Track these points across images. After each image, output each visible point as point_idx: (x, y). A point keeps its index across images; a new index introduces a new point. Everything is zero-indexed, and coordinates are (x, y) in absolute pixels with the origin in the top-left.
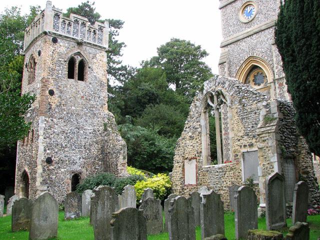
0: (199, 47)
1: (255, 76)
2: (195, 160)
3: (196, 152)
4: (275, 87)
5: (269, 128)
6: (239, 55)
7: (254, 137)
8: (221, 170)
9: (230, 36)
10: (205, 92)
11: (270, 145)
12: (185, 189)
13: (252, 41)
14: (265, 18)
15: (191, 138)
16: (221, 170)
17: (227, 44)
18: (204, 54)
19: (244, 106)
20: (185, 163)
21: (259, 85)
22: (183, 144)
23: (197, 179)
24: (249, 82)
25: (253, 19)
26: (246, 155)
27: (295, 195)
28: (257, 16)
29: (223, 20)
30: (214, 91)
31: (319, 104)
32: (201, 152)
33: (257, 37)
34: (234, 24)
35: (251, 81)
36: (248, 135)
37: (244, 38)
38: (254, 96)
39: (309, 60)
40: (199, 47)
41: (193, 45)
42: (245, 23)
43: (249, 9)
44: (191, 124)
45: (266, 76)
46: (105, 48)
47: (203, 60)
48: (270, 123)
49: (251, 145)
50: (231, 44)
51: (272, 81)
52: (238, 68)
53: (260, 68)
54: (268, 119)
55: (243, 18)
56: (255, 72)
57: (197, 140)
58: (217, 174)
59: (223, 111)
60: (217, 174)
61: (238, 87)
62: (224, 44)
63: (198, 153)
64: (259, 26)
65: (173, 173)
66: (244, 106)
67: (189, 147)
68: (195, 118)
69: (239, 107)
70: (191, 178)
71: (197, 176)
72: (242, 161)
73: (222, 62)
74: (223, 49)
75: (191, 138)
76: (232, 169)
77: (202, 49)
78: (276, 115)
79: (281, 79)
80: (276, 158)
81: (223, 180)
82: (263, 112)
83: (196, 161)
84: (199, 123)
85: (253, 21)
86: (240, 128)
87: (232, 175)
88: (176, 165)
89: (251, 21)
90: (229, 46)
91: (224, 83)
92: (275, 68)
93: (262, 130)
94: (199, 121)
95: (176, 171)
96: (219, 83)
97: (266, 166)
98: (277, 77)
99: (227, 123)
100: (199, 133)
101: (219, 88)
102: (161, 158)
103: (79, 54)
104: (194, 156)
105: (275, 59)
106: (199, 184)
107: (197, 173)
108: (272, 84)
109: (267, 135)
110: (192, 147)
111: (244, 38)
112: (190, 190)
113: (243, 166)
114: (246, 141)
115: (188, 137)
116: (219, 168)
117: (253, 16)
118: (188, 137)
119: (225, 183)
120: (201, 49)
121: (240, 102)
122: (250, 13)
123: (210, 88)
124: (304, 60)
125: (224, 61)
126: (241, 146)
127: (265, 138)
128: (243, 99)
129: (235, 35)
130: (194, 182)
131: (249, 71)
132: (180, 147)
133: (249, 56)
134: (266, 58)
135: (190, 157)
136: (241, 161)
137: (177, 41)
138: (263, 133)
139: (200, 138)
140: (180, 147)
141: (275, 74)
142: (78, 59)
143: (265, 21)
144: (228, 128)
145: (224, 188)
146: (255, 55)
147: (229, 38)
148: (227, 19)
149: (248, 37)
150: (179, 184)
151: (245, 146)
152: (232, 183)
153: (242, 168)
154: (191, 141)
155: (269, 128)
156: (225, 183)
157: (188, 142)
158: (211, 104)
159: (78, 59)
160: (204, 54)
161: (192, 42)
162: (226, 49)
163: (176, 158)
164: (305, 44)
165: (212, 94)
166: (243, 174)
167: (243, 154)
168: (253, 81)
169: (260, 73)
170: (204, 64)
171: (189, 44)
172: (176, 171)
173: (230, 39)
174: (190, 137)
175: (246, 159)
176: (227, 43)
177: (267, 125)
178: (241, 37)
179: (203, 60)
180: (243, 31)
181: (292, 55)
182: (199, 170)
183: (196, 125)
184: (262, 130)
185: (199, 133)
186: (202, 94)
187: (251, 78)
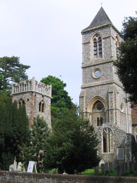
4: (109, 113)
9: (86, 83)
13: (98, 88)
17: (85, 87)
18: (65, 85)
21: (100, 110)
31: (136, 44)
34: (89, 78)
35: (96, 108)
37: (94, 86)
40: (62, 82)
42: (95, 79)
46: (50, 97)
51: (107, 109)
56: (98, 104)
62: (83, 87)
74: (83, 89)
79: (112, 110)
103: (43, 100)
108: (107, 111)
111: (94, 86)
136: (100, 142)
137: (51, 77)
141: (109, 107)
142: (42, 102)
146: (99, 96)
147: (86, 84)
148: (86, 74)
149: (97, 86)
159: (42, 102)
162: (85, 90)
165: (106, 128)
178: (93, 85)
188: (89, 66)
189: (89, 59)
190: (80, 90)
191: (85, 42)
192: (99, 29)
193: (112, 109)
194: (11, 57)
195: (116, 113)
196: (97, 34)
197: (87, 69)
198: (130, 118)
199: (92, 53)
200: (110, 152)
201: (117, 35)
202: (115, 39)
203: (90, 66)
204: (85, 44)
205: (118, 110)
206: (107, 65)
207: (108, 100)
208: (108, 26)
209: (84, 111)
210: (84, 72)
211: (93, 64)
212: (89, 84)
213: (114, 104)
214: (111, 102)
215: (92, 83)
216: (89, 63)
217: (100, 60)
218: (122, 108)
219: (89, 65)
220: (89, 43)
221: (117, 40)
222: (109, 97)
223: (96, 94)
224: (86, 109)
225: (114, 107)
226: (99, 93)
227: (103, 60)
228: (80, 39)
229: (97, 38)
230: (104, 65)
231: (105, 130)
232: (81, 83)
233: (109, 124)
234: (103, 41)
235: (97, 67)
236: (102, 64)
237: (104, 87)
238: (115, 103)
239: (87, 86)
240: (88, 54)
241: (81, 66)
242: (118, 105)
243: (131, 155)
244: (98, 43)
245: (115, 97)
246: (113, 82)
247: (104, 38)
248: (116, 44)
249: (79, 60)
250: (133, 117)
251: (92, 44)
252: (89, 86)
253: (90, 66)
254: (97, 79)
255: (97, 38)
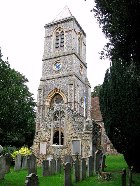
0: (24, 76)
1: (56, 99)
2: (46, 142)
3: (47, 138)
5: (89, 132)
6: (50, 87)
7: (79, 134)
8: (60, 148)
10: (54, 110)
11: (89, 138)
12: (40, 156)
14: (66, 71)
15: (45, 131)
16: (60, 148)
17: (44, 79)
18: (27, 81)
19: (75, 120)
20: (40, 143)
22: (40, 134)
23: (47, 151)
24: (53, 101)
25: (60, 70)
26: (74, 142)
27: (102, 160)
28: (62, 69)
29: (43, 67)
30: (60, 111)
32: (50, 139)
33: (61, 79)
36: (76, 133)
37: (54, 79)
38: (80, 116)
39: (117, 110)
40: (24, 76)
41: (21, 75)
42: (55, 71)
43: (58, 64)
44: (46, 124)
45: (63, 100)
47: (25, 84)
48: (89, 130)
49: (77, 138)
50: (46, 80)
51: (66, 103)
52: (49, 93)
53: (60, 95)
54: (88, 128)
55: (54, 68)
56: (57, 97)
57: (48, 133)
58: (58, 149)
59: (38, 114)
60: (58, 149)
61: (72, 111)
62: (42, 79)
63: (48, 139)
64: (62, 74)
65: (33, 147)
66: (75, 120)
67: (43, 135)
68: (48, 122)
69: (72, 120)
70: (43, 150)
71: (47, 150)
72: (72, 145)
73: (40, 89)
74: (42, 82)
75: (45, 131)
76: (66, 148)
77: (25, 78)
78: (92, 126)
79: (71, 102)
80: (91, 144)
81: (61, 152)
82: (85, 124)
83: (47, 143)
84: (50, 125)
85: (59, 71)
86: (72, 129)
87: (66, 150)
88: (34, 143)
89: (59, 70)
90: (45, 81)
91: (65, 108)
92: (68, 97)
93: (86, 132)
94: (50, 124)
95: (35, 147)
96: (63, 108)
97: (87, 147)
98: (69, 101)
99: (39, 121)
100: (50, 129)
101: (63, 110)
102: (5, 137)
104: (46, 140)
105: (69, 92)
106: (48, 154)
107: (47, 149)
109: (88, 134)
110: (45, 136)
111: (54, 79)
112: (42, 157)
113: (72, 146)
114: (74, 135)
115: (43, 131)
116: (60, 147)
117: (60, 69)
118: (43, 131)
119: (62, 154)
120: (25, 78)
121: (73, 118)
122: (58, 67)
123: (58, 109)
124: (115, 110)
125: (42, 88)
126: (72, 138)
127: (87, 136)
128: (74, 116)
129: (49, 76)
130: (45, 153)
131: (53, 96)
132: (38, 135)
133: (55, 88)
134: (64, 91)
135: (43, 140)
138: (86, 133)
139: (50, 132)
140: (38, 135)
141: (68, 100)
143: (66, 72)
144: (40, 124)
145: (62, 156)
146: (58, 88)
148: (46, 67)
149: (56, 78)
150: (36, 153)
151: (74, 138)
152: (66, 154)
153: (72, 147)
154: (45, 133)
155: (89, 132)
156: (62, 154)
157: (43, 133)
158: (57, 116)
160: (27, 81)
161: (21, 73)
162: (43, 82)
163: (35, 140)
164: (116, 104)
165: (58, 112)
166: (72, 150)
167: (73, 141)
168: (55, 101)
169: (60, 97)
170: (26, 86)
171: (19, 74)
172: (35, 147)
173: (46, 77)
174: (44, 131)
175: (74, 143)
176: (44, 79)
177: (88, 130)
179: (25, 84)
180: (53, 74)
181: (110, 107)
182: (48, 147)
183: (49, 125)
184: (86, 132)
185: (50, 129)
186: (53, 111)
187: (55, 99)
188: (50, 59)
189: (50, 52)
190: (39, 83)
191: (47, 36)
192: (62, 23)
193: (71, 101)
195: (75, 106)
196: (59, 28)
197: (48, 61)
198: (90, 114)
199: (53, 46)
200: (62, 143)
201: (79, 31)
202: (78, 34)
203: (51, 59)
204: (47, 37)
205: (78, 103)
206: (68, 57)
207: (68, 92)
208: (71, 20)
209: (79, 154)
210: (44, 64)
211: (54, 57)
212: (49, 76)
213: (73, 96)
214: (70, 95)
215: (52, 76)
216: (50, 56)
217: (60, 52)
218: (82, 103)
219: (50, 58)
220: (52, 36)
221: (79, 36)
222: (69, 90)
223: (55, 87)
224: (44, 102)
225: (73, 99)
226: (58, 85)
227: (64, 53)
228: (43, 32)
229: (60, 32)
230: (65, 57)
231: (56, 115)
232: (40, 76)
233: (62, 106)
234: (65, 34)
235: (58, 59)
236: (63, 56)
237: (63, 80)
238: (75, 95)
239: (46, 79)
240: (50, 47)
241: (42, 58)
242: (78, 98)
243: (91, 148)
244: (59, 37)
245: (75, 90)
246: (73, 74)
247: (67, 32)
248: (78, 40)
249: (40, 53)
250: (93, 114)
251: (54, 38)
252: (49, 78)
253: (51, 59)
254: (57, 71)
255: (60, 32)
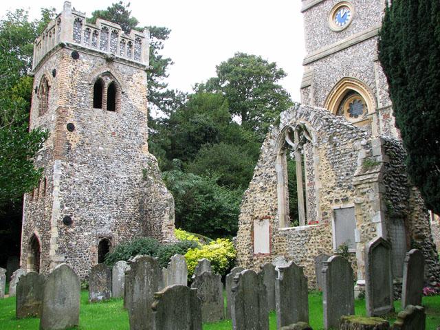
0: (274, 65)
1: (350, 105)
2: (268, 220)
3: (269, 209)
4: (379, 120)
5: (369, 176)
6: (329, 76)
7: (349, 188)
8: (303, 234)
9: (316, 49)
10: (281, 126)
11: (371, 199)
12: (255, 260)
13: (347, 56)
14: (365, 24)
15: (263, 189)
16: (303, 234)
17: (312, 60)
18: (281, 74)
19: (335, 145)
20: (255, 225)
21: (356, 116)
22: (252, 198)
23: (271, 246)
24: (343, 113)
25: (348, 26)
26: (338, 213)
27: (406, 268)
28: (353, 23)
29: (307, 28)
30: (294, 126)
32: (276, 209)
33: (353, 50)
34: (322, 34)
35: (346, 112)
36: (341, 186)
37: (335, 53)
38: (349, 132)
39: (425, 83)
40: (274, 65)
41: (265, 62)
42: (337, 32)
43: (342, 12)
44: (263, 171)
45: (366, 105)
46: (144, 66)
47: (279, 82)
48: (371, 170)
49: (345, 200)
50: (317, 60)
51: (374, 111)
52: (327, 93)
53: (358, 93)
54: (368, 164)
55: (335, 25)
56: (350, 100)
57: (271, 193)
58: (298, 239)
59: (306, 152)
60: (298, 239)
61: (327, 119)
62: (307, 61)
63: (272, 210)
64: (356, 35)
65: (238, 238)
66: (335, 145)
67: (260, 202)
68: (268, 162)
69: (329, 147)
70: (262, 245)
71: (270, 242)
72: (333, 222)
73: (305, 85)
74: (307, 67)
75: (263, 189)
76: (319, 233)
77: (278, 68)
78: (380, 159)
79: (386, 108)
80: (379, 217)
81: (307, 247)
82: (362, 154)
83: (270, 222)
84: (273, 170)
85: (347, 30)
86: (330, 176)
87: (319, 241)
88: (241, 226)
89: (346, 29)
90: (315, 63)
91: (308, 114)
92: (378, 93)
93: (361, 178)
94: (274, 167)
95: (242, 235)
96: (301, 115)
97: (366, 228)
98: (380, 106)
99: (311, 170)
100: (274, 183)
101: (301, 121)
102: (222, 218)
103: (108, 74)
104: (266, 214)
105: (378, 82)
106: (273, 253)
107: (270, 239)
108: (375, 116)
109: (368, 185)
110: (264, 202)
111: (335, 53)
112: (261, 262)
113: (334, 228)
114: (338, 193)
115: (258, 189)
116: (302, 232)
117: (348, 22)
118: (258, 189)
119: (309, 252)
120: (277, 68)
121: (330, 140)
122: (344, 18)
123: (289, 120)
124: (418, 83)
125: (308, 83)
126: (331, 201)
127: (365, 190)
128: (334, 136)
129: (323, 49)
130: (266, 250)
131: (342, 98)
132: (247, 202)
133: (342, 77)
134: (366, 80)
135: (261, 215)
136: (331, 222)
137: (243, 56)
138: (361, 182)
139: (275, 190)
140: (247, 202)
141: (379, 101)
142: (107, 81)
143: (364, 29)
144: (313, 177)
145: (308, 259)
146: (350, 76)
147: (315, 53)
148: (312, 26)
149: (341, 50)
150: (247, 253)
151: (337, 201)
152: (320, 252)
153: (333, 231)
154: (262, 194)
155: (369, 176)
156: (309, 252)
157: (258, 195)
158: (290, 143)
159: (107, 81)
160: (281, 74)
161: (263, 58)
162: (311, 68)
163: (242, 217)
164: (419, 60)
165: (291, 129)
166: (334, 240)
167: (334, 212)
168: (349, 111)
169: (358, 100)
170: (280, 87)
171: (260, 60)
172: (242, 235)
173: (317, 54)
174: (262, 188)
175: (338, 218)
176: (312, 59)
177: (368, 172)
178: (332, 51)
179: (279, 82)
180: (334, 42)
181: (401, 76)
182: (274, 234)
183: (269, 171)
184: (361, 178)
185: (274, 183)
186: (278, 129)
187: (345, 107)
194: (106, 9)
